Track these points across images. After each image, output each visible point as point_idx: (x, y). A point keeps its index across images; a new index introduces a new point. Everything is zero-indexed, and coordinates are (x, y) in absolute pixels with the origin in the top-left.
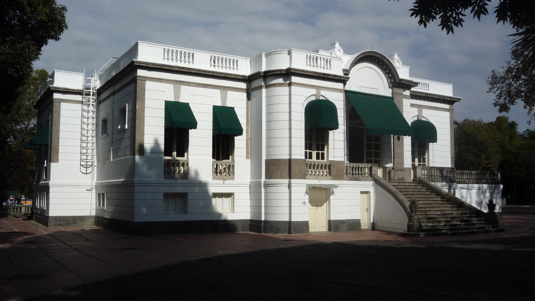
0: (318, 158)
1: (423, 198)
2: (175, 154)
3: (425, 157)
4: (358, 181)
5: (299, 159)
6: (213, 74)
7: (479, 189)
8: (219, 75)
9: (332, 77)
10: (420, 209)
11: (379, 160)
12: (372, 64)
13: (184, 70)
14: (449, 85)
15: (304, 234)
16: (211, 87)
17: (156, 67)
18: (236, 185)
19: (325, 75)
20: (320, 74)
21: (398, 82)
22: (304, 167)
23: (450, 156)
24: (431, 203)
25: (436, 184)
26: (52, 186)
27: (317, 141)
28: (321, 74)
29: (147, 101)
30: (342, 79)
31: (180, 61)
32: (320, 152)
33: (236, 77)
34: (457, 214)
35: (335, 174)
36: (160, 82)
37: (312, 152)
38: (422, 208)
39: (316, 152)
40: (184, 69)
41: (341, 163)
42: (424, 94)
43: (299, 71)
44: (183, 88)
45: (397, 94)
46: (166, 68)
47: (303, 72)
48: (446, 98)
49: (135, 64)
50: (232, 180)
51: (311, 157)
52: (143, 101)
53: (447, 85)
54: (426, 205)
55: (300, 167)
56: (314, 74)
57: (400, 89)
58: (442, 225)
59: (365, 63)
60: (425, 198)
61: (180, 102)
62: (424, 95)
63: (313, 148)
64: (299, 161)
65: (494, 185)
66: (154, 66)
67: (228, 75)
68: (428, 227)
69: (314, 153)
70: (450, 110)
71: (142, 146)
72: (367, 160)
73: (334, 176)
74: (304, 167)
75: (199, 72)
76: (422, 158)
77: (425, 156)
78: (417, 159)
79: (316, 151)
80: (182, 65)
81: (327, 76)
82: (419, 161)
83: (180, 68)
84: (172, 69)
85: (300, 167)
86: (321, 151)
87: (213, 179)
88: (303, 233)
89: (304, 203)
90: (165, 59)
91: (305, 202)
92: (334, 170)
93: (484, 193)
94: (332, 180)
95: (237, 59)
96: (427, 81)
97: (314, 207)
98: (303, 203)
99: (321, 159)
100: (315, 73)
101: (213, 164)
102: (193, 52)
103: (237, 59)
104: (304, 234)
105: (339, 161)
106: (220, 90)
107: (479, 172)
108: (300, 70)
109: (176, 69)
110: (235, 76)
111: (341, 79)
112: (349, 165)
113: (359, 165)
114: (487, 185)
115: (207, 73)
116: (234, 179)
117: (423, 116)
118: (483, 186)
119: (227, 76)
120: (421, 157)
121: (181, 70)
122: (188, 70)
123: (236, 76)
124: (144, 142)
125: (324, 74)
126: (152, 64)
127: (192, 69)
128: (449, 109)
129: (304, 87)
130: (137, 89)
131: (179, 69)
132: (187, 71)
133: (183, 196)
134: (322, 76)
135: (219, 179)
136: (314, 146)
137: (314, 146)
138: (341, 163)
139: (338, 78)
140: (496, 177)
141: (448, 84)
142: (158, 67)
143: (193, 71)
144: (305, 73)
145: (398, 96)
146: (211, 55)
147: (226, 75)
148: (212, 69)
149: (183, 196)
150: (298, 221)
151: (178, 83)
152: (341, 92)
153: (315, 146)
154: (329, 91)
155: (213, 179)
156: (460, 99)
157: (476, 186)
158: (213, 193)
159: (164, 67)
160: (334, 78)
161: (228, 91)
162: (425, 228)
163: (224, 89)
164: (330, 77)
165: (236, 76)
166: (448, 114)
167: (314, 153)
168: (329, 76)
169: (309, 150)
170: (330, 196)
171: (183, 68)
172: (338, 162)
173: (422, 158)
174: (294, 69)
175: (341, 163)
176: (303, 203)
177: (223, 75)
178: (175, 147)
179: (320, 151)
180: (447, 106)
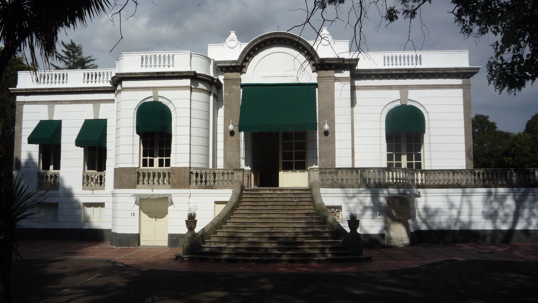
0: (161, 164)
1: (275, 211)
2: (51, 167)
3: (420, 154)
4: (211, 189)
5: (128, 168)
6: (82, 90)
7: (489, 194)
8: (87, 90)
9: (170, 75)
10: (245, 225)
11: (304, 161)
12: (265, 50)
13: (54, 91)
14: (460, 52)
15: (132, 247)
16: (83, 103)
17: (29, 91)
18: (200, 195)
19: (160, 74)
20: (153, 74)
21: (319, 62)
22: (134, 176)
23: (464, 150)
24: (274, 215)
25: (346, 190)
26: (194, 195)
27: (160, 147)
28: (155, 74)
29: (24, 122)
30: (183, 74)
31: (404, 64)
32: (164, 158)
33: (105, 89)
34: (292, 232)
35: (176, 182)
36: (36, 104)
37: (153, 159)
38: (248, 224)
39: (159, 159)
40: (54, 90)
41: (185, 170)
42: (406, 71)
43: (126, 75)
44: (102, 105)
45: (323, 78)
46: (38, 91)
47: (132, 74)
48: (448, 70)
49: (11, 92)
50: (102, 190)
51: (152, 164)
52: (21, 123)
53: (457, 52)
54: (263, 219)
55: (130, 175)
56: (146, 75)
57: (329, 71)
58: (232, 248)
59: (266, 50)
60: (280, 211)
61: (54, 119)
62: (407, 72)
63: (155, 155)
64: (128, 169)
65: (522, 189)
66: (27, 91)
67: (96, 88)
68: (212, 249)
69: (156, 160)
70: (463, 86)
71: (18, 162)
72: (283, 162)
73: (174, 184)
74: (134, 176)
75: (68, 90)
76: (414, 155)
77: (420, 151)
78: (406, 156)
79: (158, 158)
80: (53, 86)
81: (162, 75)
82: (409, 158)
83: (50, 90)
84: (43, 91)
85: (130, 176)
86: (165, 157)
87: (83, 190)
88: (131, 247)
89: (133, 214)
90: (394, 65)
91: (134, 213)
92: (174, 178)
93: (501, 200)
94: (171, 189)
95: (111, 71)
96: (389, 54)
97: (152, 218)
98: (132, 214)
99: (166, 166)
100: (146, 74)
101: (83, 175)
102: (67, 72)
103: (67, 72)
104: (132, 247)
105: (182, 168)
106: (92, 104)
107: (490, 170)
108: (127, 74)
109: (47, 91)
110: (104, 88)
111: (181, 74)
112: (200, 171)
113: (214, 171)
114: (506, 189)
115: (75, 90)
116: (104, 189)
117: (409, 100)
118: (496, 190)
119: (96, 89)
120: (413, 154)
121: (52, 91)
122: (58, 90)
123: (105, 88)
124: (21, 158)
125: (158, 73)
126: (25, 90)
127: (61, 89)
128: (461, 85)
129: (137, 91)
130: (16, 113)
131: (49, 91)
132: (56, 91)
133: (55, 205)
134: (156, 75)
135: (88, 189)
136: (156, 152)
137: (156, 152)
138: (184, 169)
139: (178, 74)
140: (531, 177)
141: (460, 51)
142: (31, 91)
143: (62, 91)
144: (134, 76)
145: (326, 80)
146: (84, 72)
147: (95, 89)
148: (86, 85)
149: (55, 205)
150: (125, 234)
151: (52, 103)
152: (186, 89)
153: (158, 151)
154: (170, 90)
155: (83, 190)
156: (479, 69)
157: (484, 190)
158: (83, 203)
159: (36, 91)
160: (172, 75)
161: (101, 104)
162: (207, 249)
163: (96, 102)
164: (167, 75)
165: (105, 88)
166: (460, 92)
167: (156, 160)
168: (165, 74)
169: (149, 157)
170: (168, 207)
171: (53, 89)
172: (180, 168)
173: (414, 155)
174: (120, 74)
175: (185, 170)
176: (132, 214)
177: (92, 90)
178: (52, 160)
179: (163, 157)
180: (459, 82)
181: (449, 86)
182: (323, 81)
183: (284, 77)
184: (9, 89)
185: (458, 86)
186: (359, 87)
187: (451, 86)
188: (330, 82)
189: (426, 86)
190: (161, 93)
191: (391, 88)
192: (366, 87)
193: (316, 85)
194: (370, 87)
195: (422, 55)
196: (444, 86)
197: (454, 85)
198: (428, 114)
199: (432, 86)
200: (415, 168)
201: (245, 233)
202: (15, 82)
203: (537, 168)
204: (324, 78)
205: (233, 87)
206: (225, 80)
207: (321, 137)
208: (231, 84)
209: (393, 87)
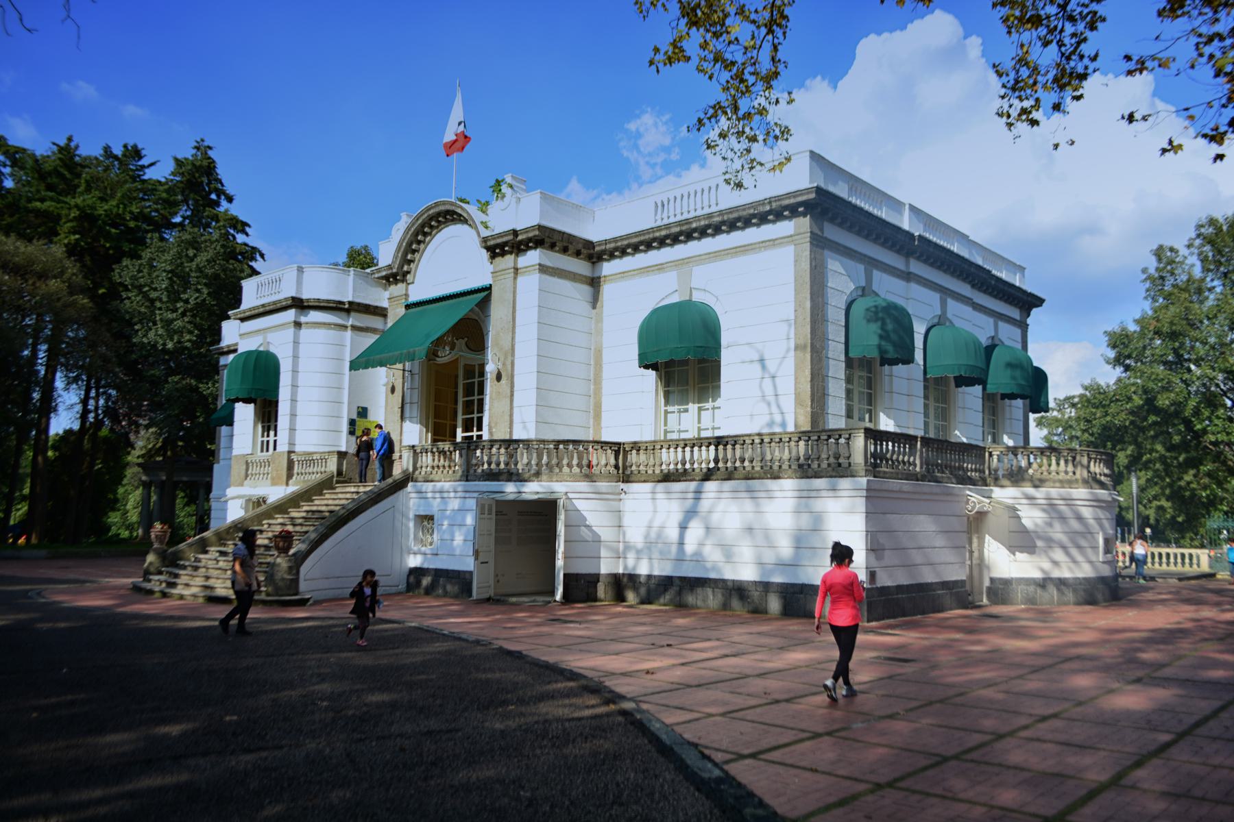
70: (794, 238)
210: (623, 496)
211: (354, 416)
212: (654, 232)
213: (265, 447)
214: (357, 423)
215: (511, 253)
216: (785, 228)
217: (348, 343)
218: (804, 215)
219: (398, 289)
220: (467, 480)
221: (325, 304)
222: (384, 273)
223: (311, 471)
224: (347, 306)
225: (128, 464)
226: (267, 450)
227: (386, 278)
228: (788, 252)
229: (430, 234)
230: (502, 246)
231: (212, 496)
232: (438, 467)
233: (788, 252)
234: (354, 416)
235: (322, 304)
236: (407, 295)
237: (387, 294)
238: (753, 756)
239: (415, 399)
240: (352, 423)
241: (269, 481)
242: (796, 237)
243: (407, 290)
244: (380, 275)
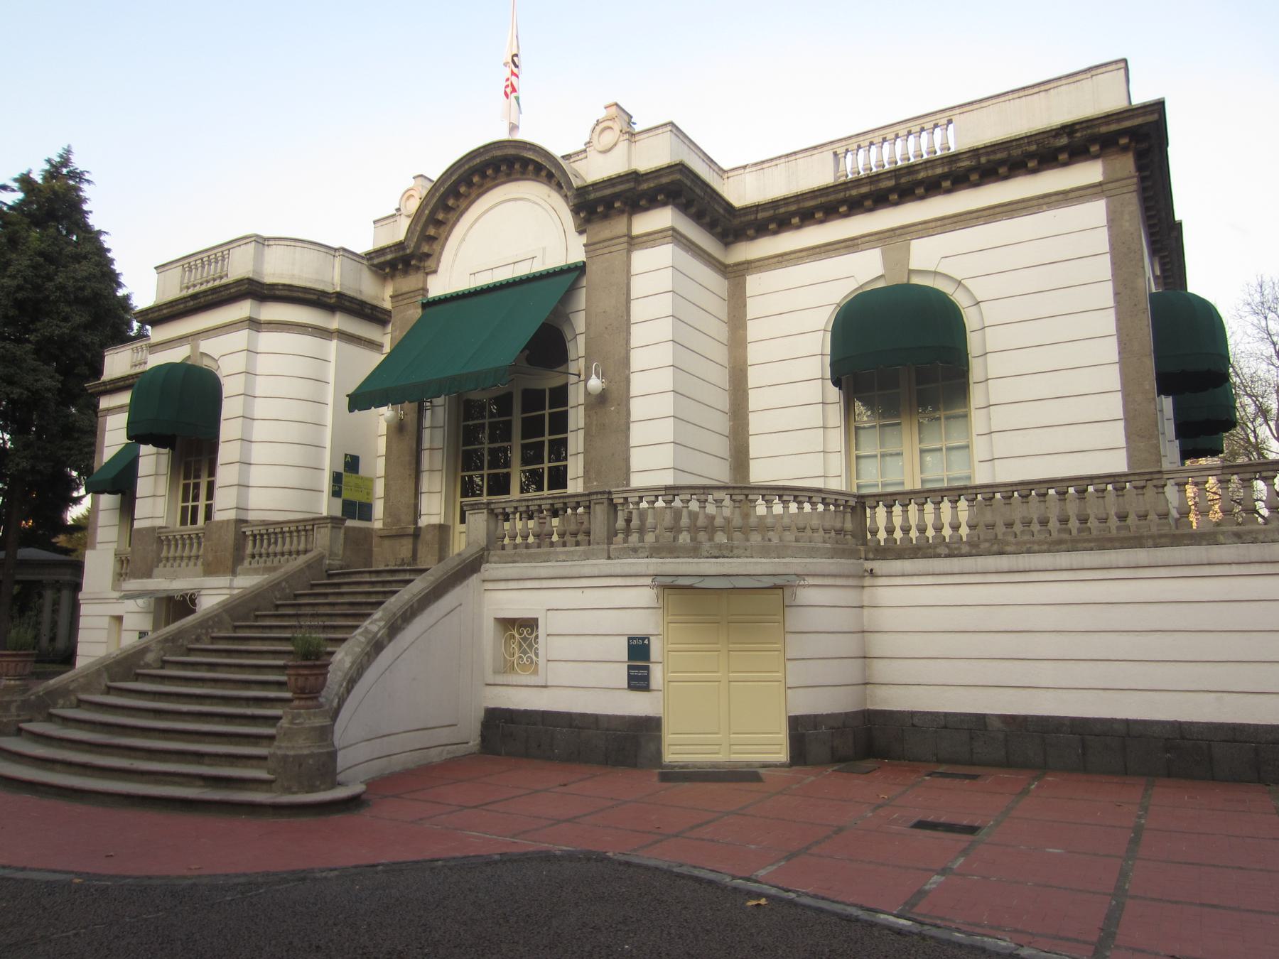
70: (1105, 187)
128: (1100, 184)
145: (606, 250)
181: (1053, 198)
182: (600, 252)
183: (514, 263)
184: (86, 385)
185: (1089, 191)
186: (761, 263)
187: (1060, 197)
188: (615, 254)
189: (969, 216)
190: (206, 346)
191: (853, 246)
192: (780, 259)
193: (578, 270)
194: (793, 256)
195: (899, 132)
196: (1035, 202)
197: (1072, 190)
198: (965, 287)
199: (991, 212)
200: (354, 529)
201: (1125, 634)
202: (98, 371)
203: (6, 873)
204: (601, 245)
205: (408, 313)
206: (395, 300)
207: (589, 416)
208: (406, 306)
209: (859, 241)
210: (868, 581)
211: (341, 469)
212: (848, 189)
213: (189, 516)
214: (344, 479)
215: (621, 212)
216: (1089, 173)
217: (333, 358)
218: (1125, 149)
219: (409, 283)
220: (609, 558)
221: (301, 295)
222: (389, 257)
223: (279, 549)
224: (333, 301)
225: (746, 234)
226: (194, 521)
227: (392, 265)
228: (1096, 211)
229: (466, 196)
230: (608, 203)
231: (81, 596)
232: (261, 555)
233: (1096, 211)
234: (341, 469)
235: (295, 294)
236: (425, 290)
237: (389, 291)
238: (567, 820)
239: (439, 443)
240: (337, 478)
241: (200, 567)
242: (1110, 186)
243: (425, 282)
244: (382, 259)
